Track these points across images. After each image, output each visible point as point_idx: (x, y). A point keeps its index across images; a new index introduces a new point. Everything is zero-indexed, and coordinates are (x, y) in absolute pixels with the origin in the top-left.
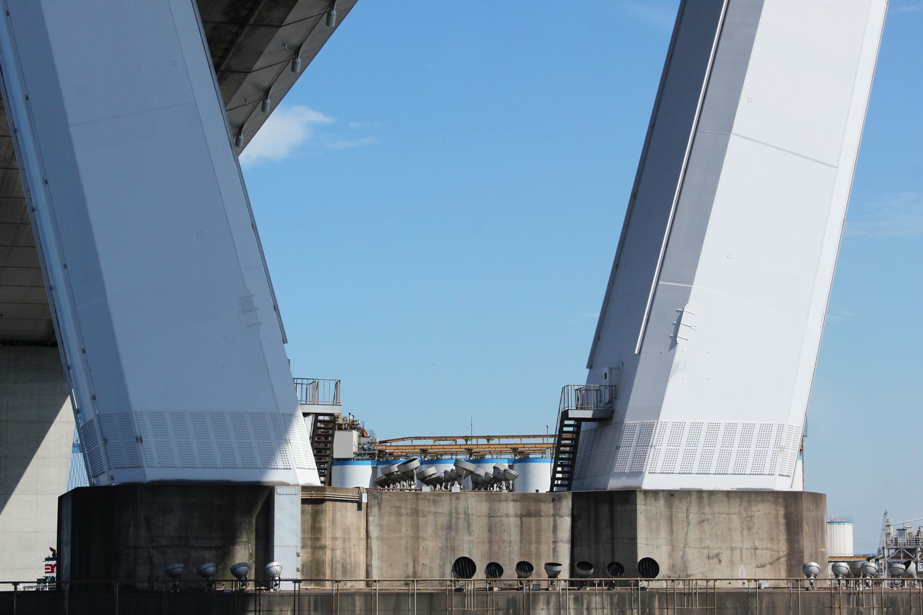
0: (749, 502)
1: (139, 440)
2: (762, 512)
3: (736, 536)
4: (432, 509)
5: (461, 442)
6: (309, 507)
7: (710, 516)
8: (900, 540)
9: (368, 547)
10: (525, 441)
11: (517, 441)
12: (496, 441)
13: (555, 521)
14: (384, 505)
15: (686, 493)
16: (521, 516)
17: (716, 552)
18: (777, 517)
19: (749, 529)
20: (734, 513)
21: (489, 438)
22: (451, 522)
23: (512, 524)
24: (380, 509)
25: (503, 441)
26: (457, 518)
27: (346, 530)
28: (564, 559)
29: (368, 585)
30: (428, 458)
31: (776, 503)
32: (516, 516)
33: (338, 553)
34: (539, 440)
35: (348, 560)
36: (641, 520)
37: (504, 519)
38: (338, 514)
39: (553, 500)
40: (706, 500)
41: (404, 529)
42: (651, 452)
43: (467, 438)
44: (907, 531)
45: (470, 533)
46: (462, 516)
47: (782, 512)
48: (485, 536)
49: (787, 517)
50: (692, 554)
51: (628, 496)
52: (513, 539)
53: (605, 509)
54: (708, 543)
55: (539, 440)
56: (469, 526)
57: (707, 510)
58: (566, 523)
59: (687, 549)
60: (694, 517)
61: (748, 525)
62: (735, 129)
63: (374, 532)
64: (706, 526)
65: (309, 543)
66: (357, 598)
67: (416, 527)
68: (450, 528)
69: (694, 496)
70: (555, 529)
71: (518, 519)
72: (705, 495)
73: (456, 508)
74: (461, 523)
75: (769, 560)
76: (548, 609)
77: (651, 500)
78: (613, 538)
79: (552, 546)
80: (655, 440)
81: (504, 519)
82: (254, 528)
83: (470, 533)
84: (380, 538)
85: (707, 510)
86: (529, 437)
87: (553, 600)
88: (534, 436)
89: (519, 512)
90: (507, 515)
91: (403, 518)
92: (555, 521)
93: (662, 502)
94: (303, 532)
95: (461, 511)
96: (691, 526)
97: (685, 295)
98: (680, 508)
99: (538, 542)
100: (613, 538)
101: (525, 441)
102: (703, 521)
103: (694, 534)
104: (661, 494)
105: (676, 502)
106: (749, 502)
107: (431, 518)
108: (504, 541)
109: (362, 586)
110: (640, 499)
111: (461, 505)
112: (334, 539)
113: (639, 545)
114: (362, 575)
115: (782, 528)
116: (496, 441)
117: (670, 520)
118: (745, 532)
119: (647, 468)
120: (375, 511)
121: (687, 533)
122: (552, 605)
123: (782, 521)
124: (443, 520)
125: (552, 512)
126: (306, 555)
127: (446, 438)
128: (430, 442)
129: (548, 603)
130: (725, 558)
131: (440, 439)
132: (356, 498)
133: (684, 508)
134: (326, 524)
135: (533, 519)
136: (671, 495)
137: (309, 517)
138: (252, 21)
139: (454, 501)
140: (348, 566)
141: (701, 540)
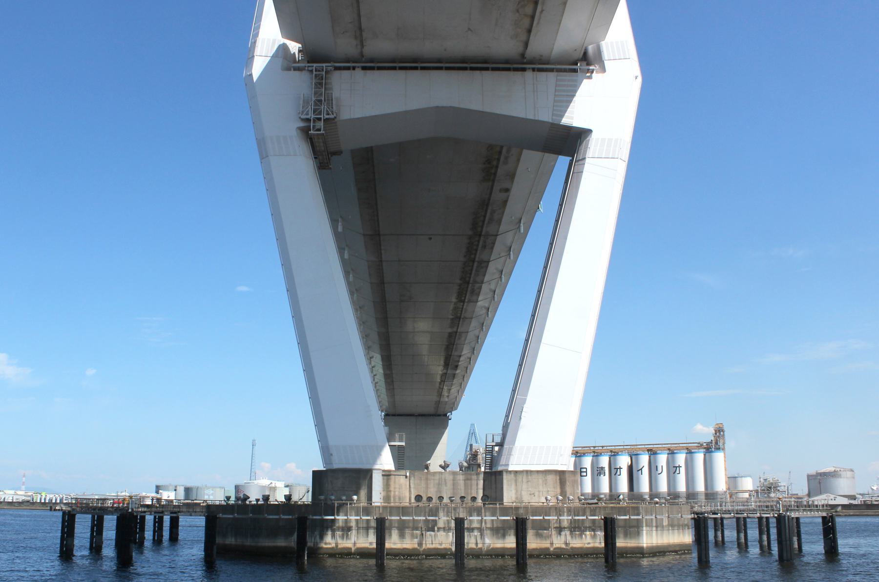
0: (546, 474)
1: (332, 455)
2: (550, 478)
3: (541, 487)
4: (433, 478)
5: (592, 448)
6: (385, 477)
7: (530, 480)
8: (765, 484)
9: (410, 491)
10: (690, 445)
11: (669, 446)
12: (605, 448)
13: (477, 482)
14: (416, 476)
15: (522, 472)
16: (465, 480)
17: (533, 492)
18: (556, 480)
19: (546, 484)
20: (540, 479)
21: (603, 447)
22: (439, 482)
23: (462, 483)
24: (414, 478)
25: (608, 448)
26: (442, 481)
27: (400, 485)
28: (481, 494)
29: (410, 504)
30: (613, 454)
31: (556, 475)
32: (463, 480)
33: (397, 493)
34: (622, 447)
35: (401, 495)
36: (505, 481)
37: (459, 481)
38: (397, 480)
39: (477, 474)
40: (529, 474)
41: (422, 485)
42: (512, 457)
43: (594, 447)
44: (768, 480)
45: (446, 486)
46: (443, 480)
47: (558, 478)
48: (452, 487)
49: (560, 479)
50: (524, 493)
51: (501, 473)
52: (462, 488)
53: (493, 477)
54: (530, 489)
55: (622, 447)
56: (446, 484)
57: (529, 477)
58: (481, 482)
59: (522, 492)
60: (525, 480)
61: (545, 482)
62: (542, 341)
63: (412, 486)
64: (529, 483)
65: (385, 489)
66: (377, 508)
67: (427, 484)
68: (439, 484)
69: (525, 473)
70: (477, 484)
71: (464, 481)
72: (529, 472)
73: (442, 478)
74: (443, 482)
75: (553, 495)
76: (444, 512)
77: (509, 474)
78: (496, 488)
79: (476, 491)
80: (513, 453)
81: (459, 481)
82: (367, 484)
83: (446, 486)
84: (414, 488)
85: (529, 477)
86: (665, 444)
87: (446, 509)
88: (620, 446)
89: (464, 479)
90: (460, 480)
91: (422, 481)
92: (477, 482)
93: (513, 475)
94: (384, 485)
95: (443, 478)
96: (524, 483)
97: (524, 401)
98: (520, 477)
99: (471, 489)
100: (496, 488)
101: (690, 445)
102: (528, 482)
103: (524, 486)
104: (512, 472)
105: (518, 474)
106: (546, 474)
107: (432, 481)
108: (459, 489)
109: (408, 504)
110: (504, 474)
111: (443, 476)
112: (395, 488)
113: (504, 490)
114: (408, 501)
115: (558, 484)
116: (605, 448)
117: (516, 481)
118: (544, 485)
119: (510, 463)
120: (412, 478)
121: (522, 486)
122: (445, 511)
123: (558, 481)
124: (437, 482)
125: (476, 478)
126: (383, 494)
127: (586, 447)
128: (580, 449)
129: (444, 510)
130: (537, 494)
131: (584, 447)
132: (405, 474)
133: (521, 477)
134: (392, 483)
135: (469, 481)
136: (516, 472)
137: (385, 481)
138: (466, 300)
139: (441, 475)
140: (401, 498)
141: (527, 488)
